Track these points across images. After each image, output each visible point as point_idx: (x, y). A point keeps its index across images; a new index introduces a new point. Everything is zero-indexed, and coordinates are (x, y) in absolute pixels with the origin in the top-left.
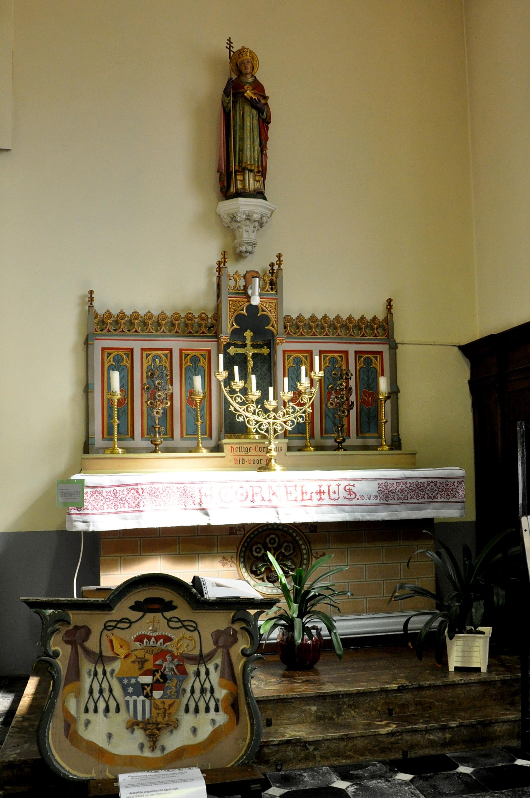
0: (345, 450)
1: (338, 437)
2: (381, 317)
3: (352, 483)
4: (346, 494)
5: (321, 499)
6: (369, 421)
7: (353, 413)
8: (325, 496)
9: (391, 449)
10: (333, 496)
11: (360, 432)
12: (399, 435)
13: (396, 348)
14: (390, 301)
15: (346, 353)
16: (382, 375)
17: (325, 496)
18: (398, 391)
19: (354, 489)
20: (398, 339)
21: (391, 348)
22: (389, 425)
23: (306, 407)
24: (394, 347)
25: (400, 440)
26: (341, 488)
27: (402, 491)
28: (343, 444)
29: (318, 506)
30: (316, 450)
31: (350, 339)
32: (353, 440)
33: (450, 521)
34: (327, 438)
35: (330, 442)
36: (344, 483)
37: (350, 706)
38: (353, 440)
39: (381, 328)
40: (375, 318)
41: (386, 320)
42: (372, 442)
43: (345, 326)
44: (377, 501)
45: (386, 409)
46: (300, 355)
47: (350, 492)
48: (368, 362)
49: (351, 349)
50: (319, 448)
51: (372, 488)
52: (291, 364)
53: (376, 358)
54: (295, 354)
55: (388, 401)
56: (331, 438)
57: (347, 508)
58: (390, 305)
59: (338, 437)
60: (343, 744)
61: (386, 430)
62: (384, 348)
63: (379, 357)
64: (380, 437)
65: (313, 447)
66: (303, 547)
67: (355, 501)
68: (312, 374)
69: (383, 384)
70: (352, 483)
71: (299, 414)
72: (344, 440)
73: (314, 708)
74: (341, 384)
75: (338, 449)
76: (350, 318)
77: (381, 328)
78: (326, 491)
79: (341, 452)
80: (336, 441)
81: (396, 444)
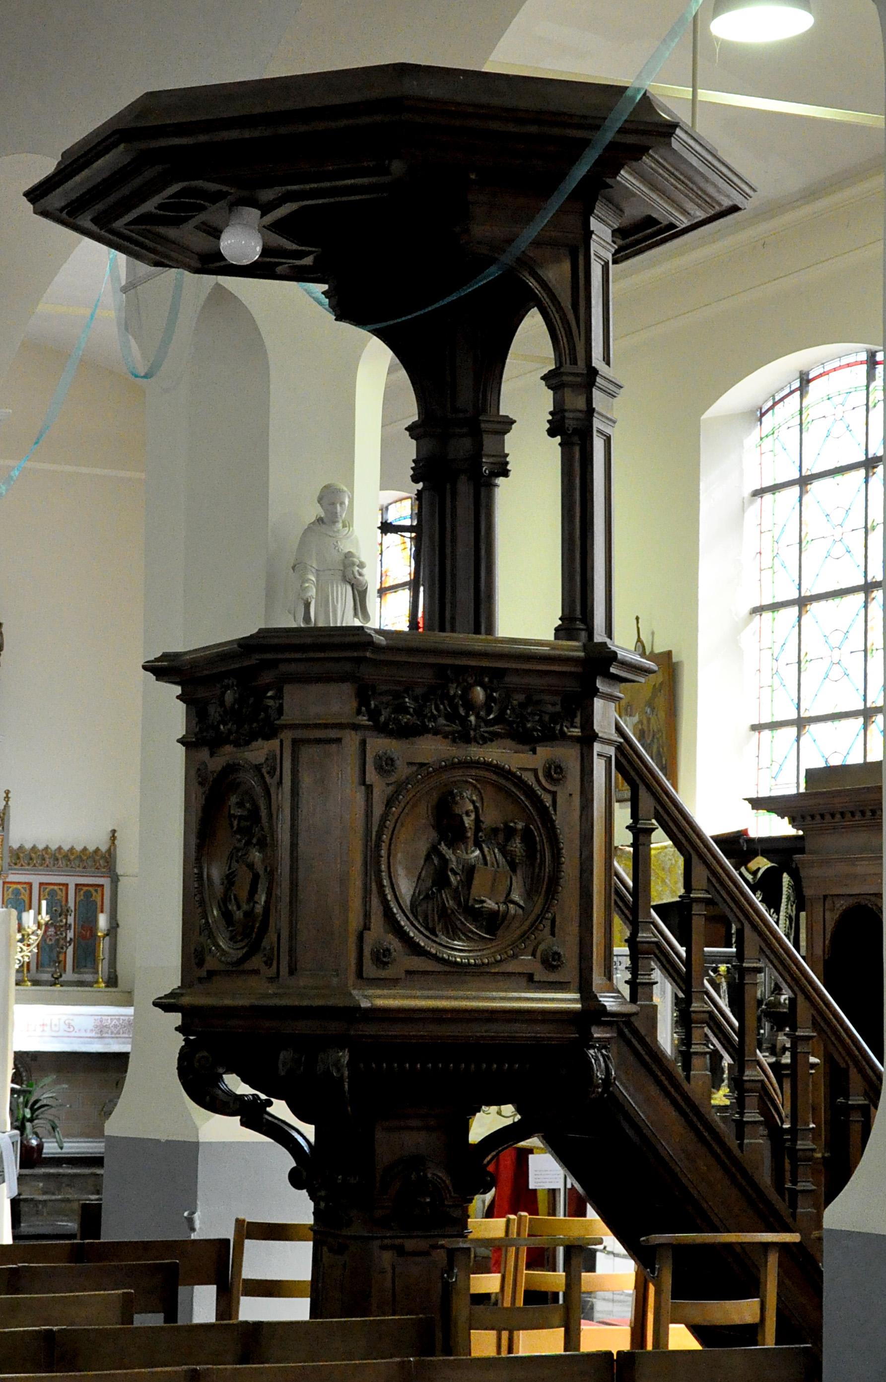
0: (62, 986)
1: (56, 972)
2: (104, 848)
3: (71, 1017)
4: (66, 1028)
5: (43, 1031)
6: (86, 955)
7: (70, 950)
8: (47, 1028)
9: (107, 986)
10: (54, 1028)
11: (76, 968)
12: (115, 971)
13: (118, 880)
14: (114, 831)
15: (67, 885)
16: (102, 912)
17: (47, 1028)
18: (118, 925)
19: (72, 1023)
20: (120, 870)
21: (112, 882)
22: (106, 962)
23: (32, 947)
24: (115, 880)
25: (116, 977)
26: (62, 1021)
27: (115, 1026)
28: (61, 979)
29: (41, 1036)
30: (33, 985)
31: (71, 871)
32: (69, 975)
33: (10, 1013)
34: (43, 972)
35: (46, 977)
36: (65, 1017)
37: (68, 1185)
38: (69, 975)
39: (104, 861)
40: (97, 850)
41: (109, 850)
42: (88, 977)
43: (66, 857)
44: (93, 1034)
45: (103, 947)
46: (19, 886)
47: (69, 1026)
48: (88, 895)
49: (72, 881)
50: (36, 983)
51: (90, 1023)
52: (10, 896)
53: (96, 891)
54: (15, 886)
55: (107, 938)
56: (48, 972)
57: (66, 1039)
58: (113, 836)
59: (56, 972)
60: (63, 1205)
61: (103, 967)
62: (105, 881)
63: (99, 889)
64: (97, 973)
65: (29, 981)
66: (24, 1074)
67: (73, 1034)
68: (39, 917)
69: (103, 921)
70: (71, 1017)
71: (26, 953)
72: (61, 976)
73: (41, 1185)
74: (61, 921)
75: (54, 984)
76: (72, 849)
77: (104, 861)
78: (49, 1023)
79: (58, 987)
80: (52, 976)
81: (112, 981)
